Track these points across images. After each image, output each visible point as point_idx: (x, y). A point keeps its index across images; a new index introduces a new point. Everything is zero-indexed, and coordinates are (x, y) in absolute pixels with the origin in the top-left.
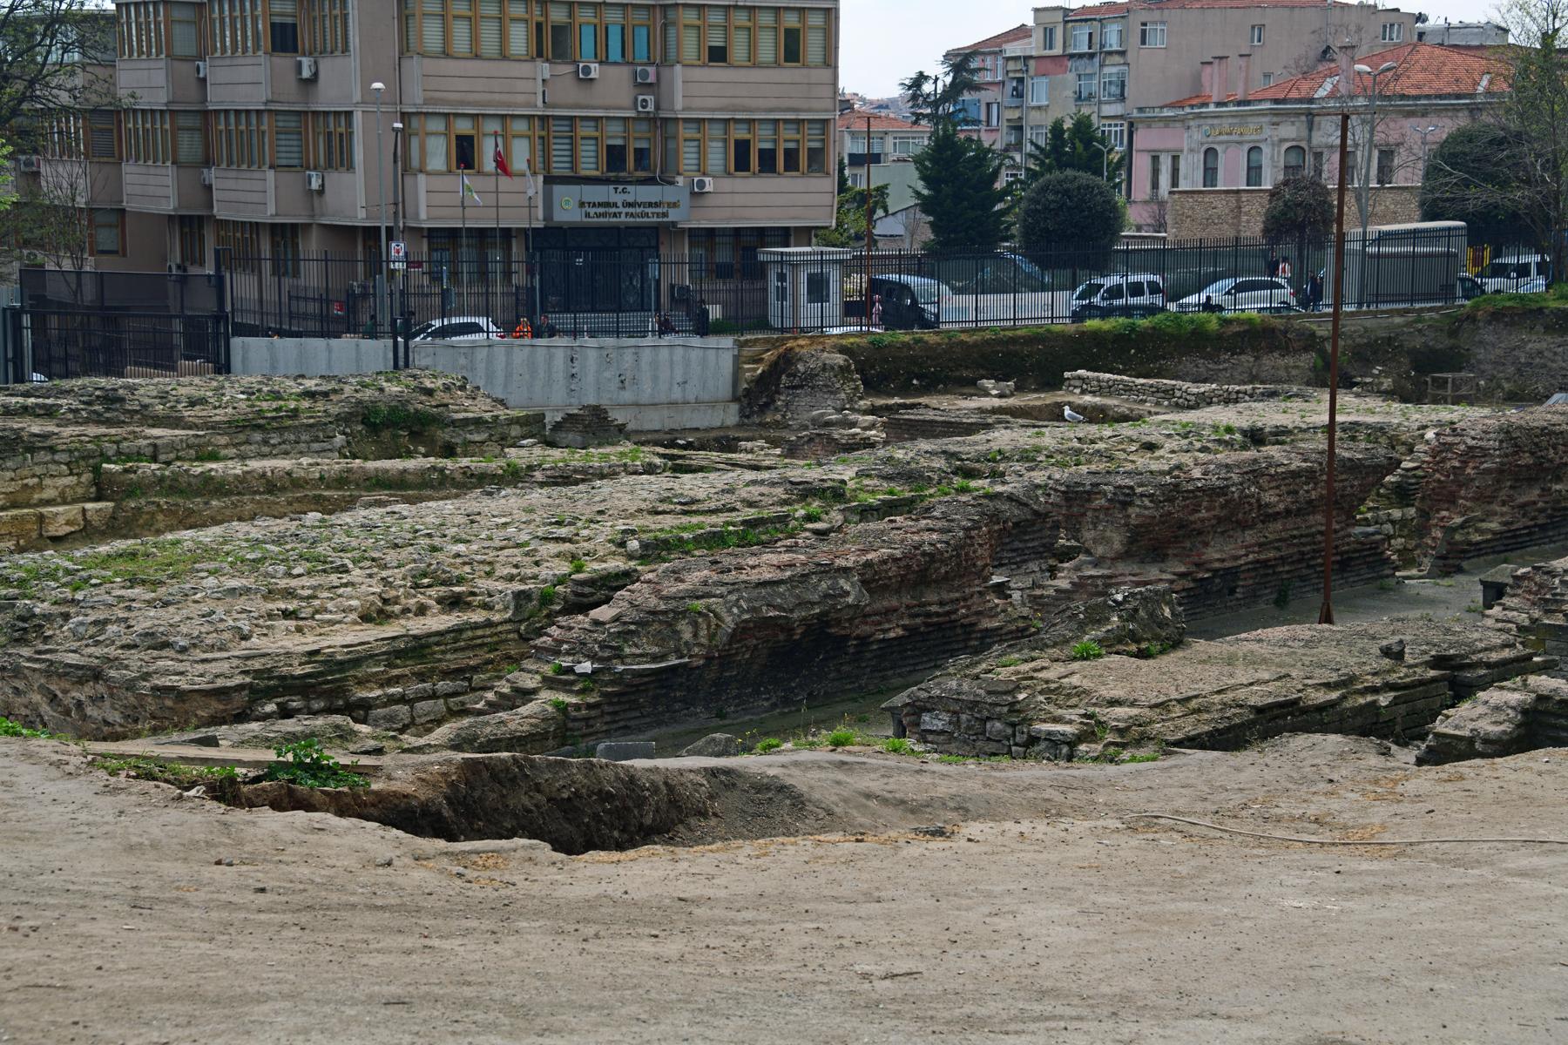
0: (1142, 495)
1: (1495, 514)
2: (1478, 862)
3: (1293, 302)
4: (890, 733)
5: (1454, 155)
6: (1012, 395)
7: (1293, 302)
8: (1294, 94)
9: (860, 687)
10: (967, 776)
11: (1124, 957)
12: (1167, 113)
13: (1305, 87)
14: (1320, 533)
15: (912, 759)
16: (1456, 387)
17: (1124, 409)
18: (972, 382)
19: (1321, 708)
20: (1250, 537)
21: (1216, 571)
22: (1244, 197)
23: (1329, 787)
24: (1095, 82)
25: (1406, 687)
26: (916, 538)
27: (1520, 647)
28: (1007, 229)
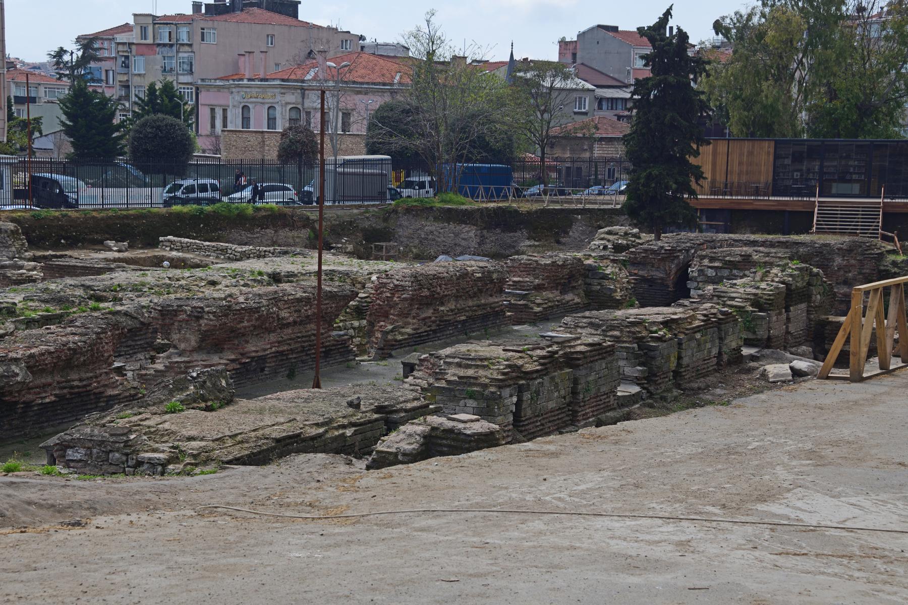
0: (208, 312)
1: (409, 323)
2: (399, 524)
3: (296, 199)
4: (45, 462)
5: (383, 117)
6: (126, 250)
7: (296, 199)
8: (293, 77)
9: (25, 434)
10: (97, 487)
11: (194, 594)
12: (219, 83)
13: (299, 72)
14: (314, 335)
15: (59, 478)
16: (388, 251)
17: (197, 261)
18: (101, 242)
19: (313, 438)
20: (273, 337)
21: (253, 357)
23: (318, 485)
24: (174, 61)
25: (361, 424)
26: (64, 339)
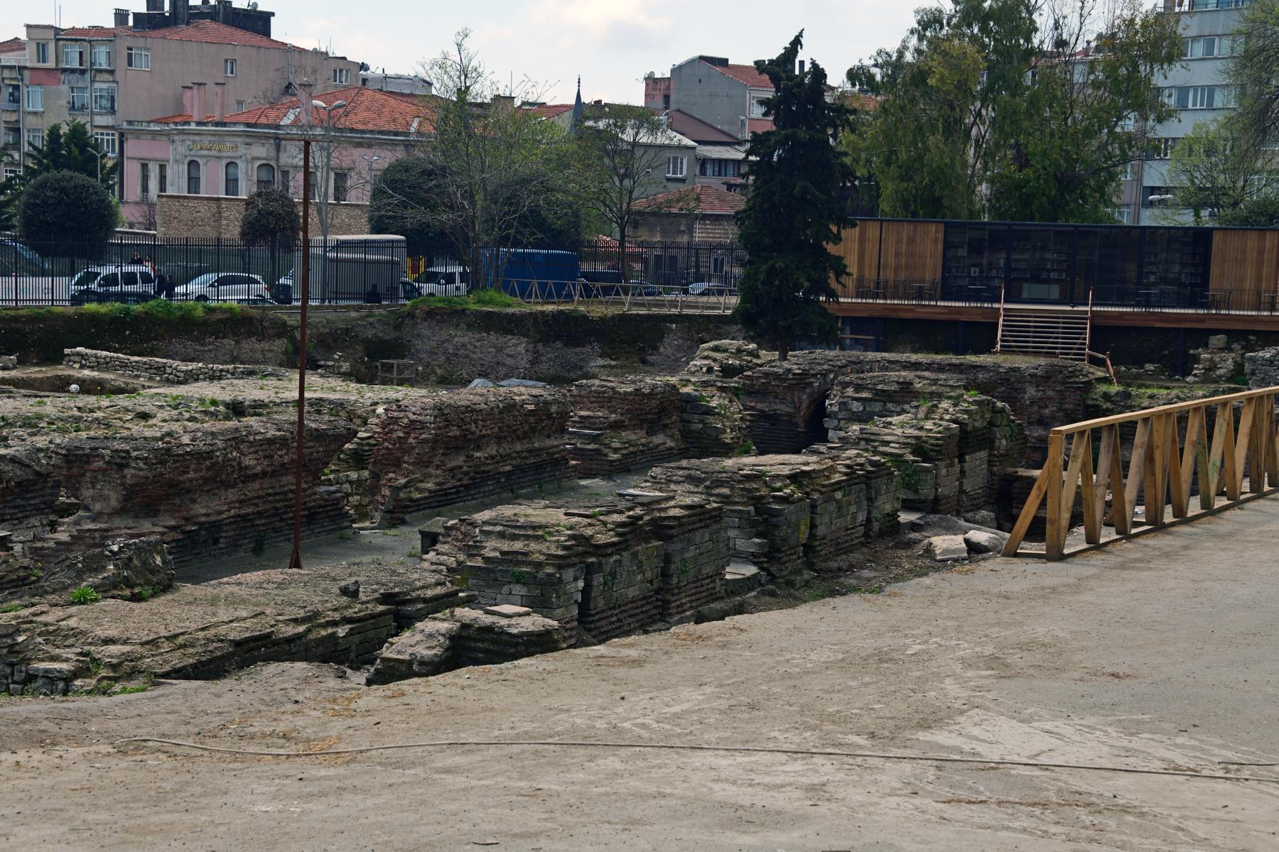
0: (137, 458)
1: (431, 476)
2: (413, 763)
3: (268, 295)
6: (14, 368)
7: (268, 295)
8: (263, 120)
12: (153, 127)
13: (272, 114)
14: (291, 491)
16: (400, 372)
17: (120, 382)
19: (289, 640)
20: (232, 494)
21: (202, 524)
22: (224, 204)
23: (296, 707)
24: (87, 95)
27: (449, 584)
28: (8, 219)
